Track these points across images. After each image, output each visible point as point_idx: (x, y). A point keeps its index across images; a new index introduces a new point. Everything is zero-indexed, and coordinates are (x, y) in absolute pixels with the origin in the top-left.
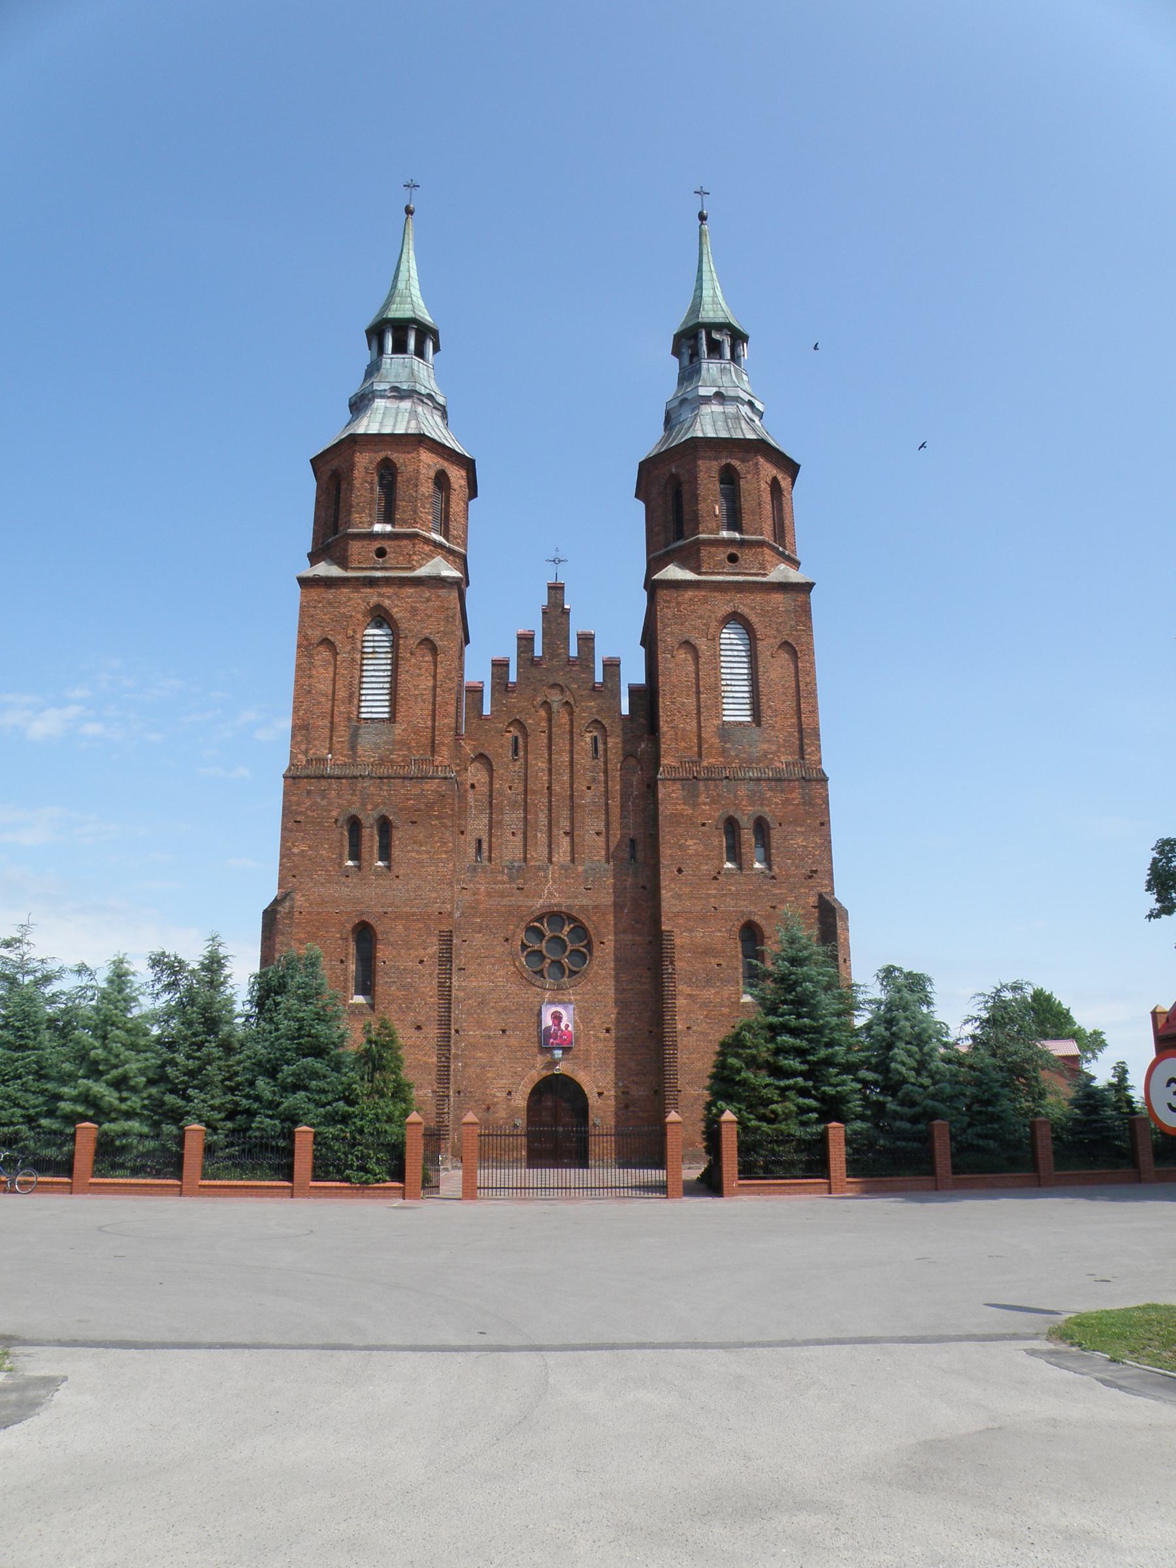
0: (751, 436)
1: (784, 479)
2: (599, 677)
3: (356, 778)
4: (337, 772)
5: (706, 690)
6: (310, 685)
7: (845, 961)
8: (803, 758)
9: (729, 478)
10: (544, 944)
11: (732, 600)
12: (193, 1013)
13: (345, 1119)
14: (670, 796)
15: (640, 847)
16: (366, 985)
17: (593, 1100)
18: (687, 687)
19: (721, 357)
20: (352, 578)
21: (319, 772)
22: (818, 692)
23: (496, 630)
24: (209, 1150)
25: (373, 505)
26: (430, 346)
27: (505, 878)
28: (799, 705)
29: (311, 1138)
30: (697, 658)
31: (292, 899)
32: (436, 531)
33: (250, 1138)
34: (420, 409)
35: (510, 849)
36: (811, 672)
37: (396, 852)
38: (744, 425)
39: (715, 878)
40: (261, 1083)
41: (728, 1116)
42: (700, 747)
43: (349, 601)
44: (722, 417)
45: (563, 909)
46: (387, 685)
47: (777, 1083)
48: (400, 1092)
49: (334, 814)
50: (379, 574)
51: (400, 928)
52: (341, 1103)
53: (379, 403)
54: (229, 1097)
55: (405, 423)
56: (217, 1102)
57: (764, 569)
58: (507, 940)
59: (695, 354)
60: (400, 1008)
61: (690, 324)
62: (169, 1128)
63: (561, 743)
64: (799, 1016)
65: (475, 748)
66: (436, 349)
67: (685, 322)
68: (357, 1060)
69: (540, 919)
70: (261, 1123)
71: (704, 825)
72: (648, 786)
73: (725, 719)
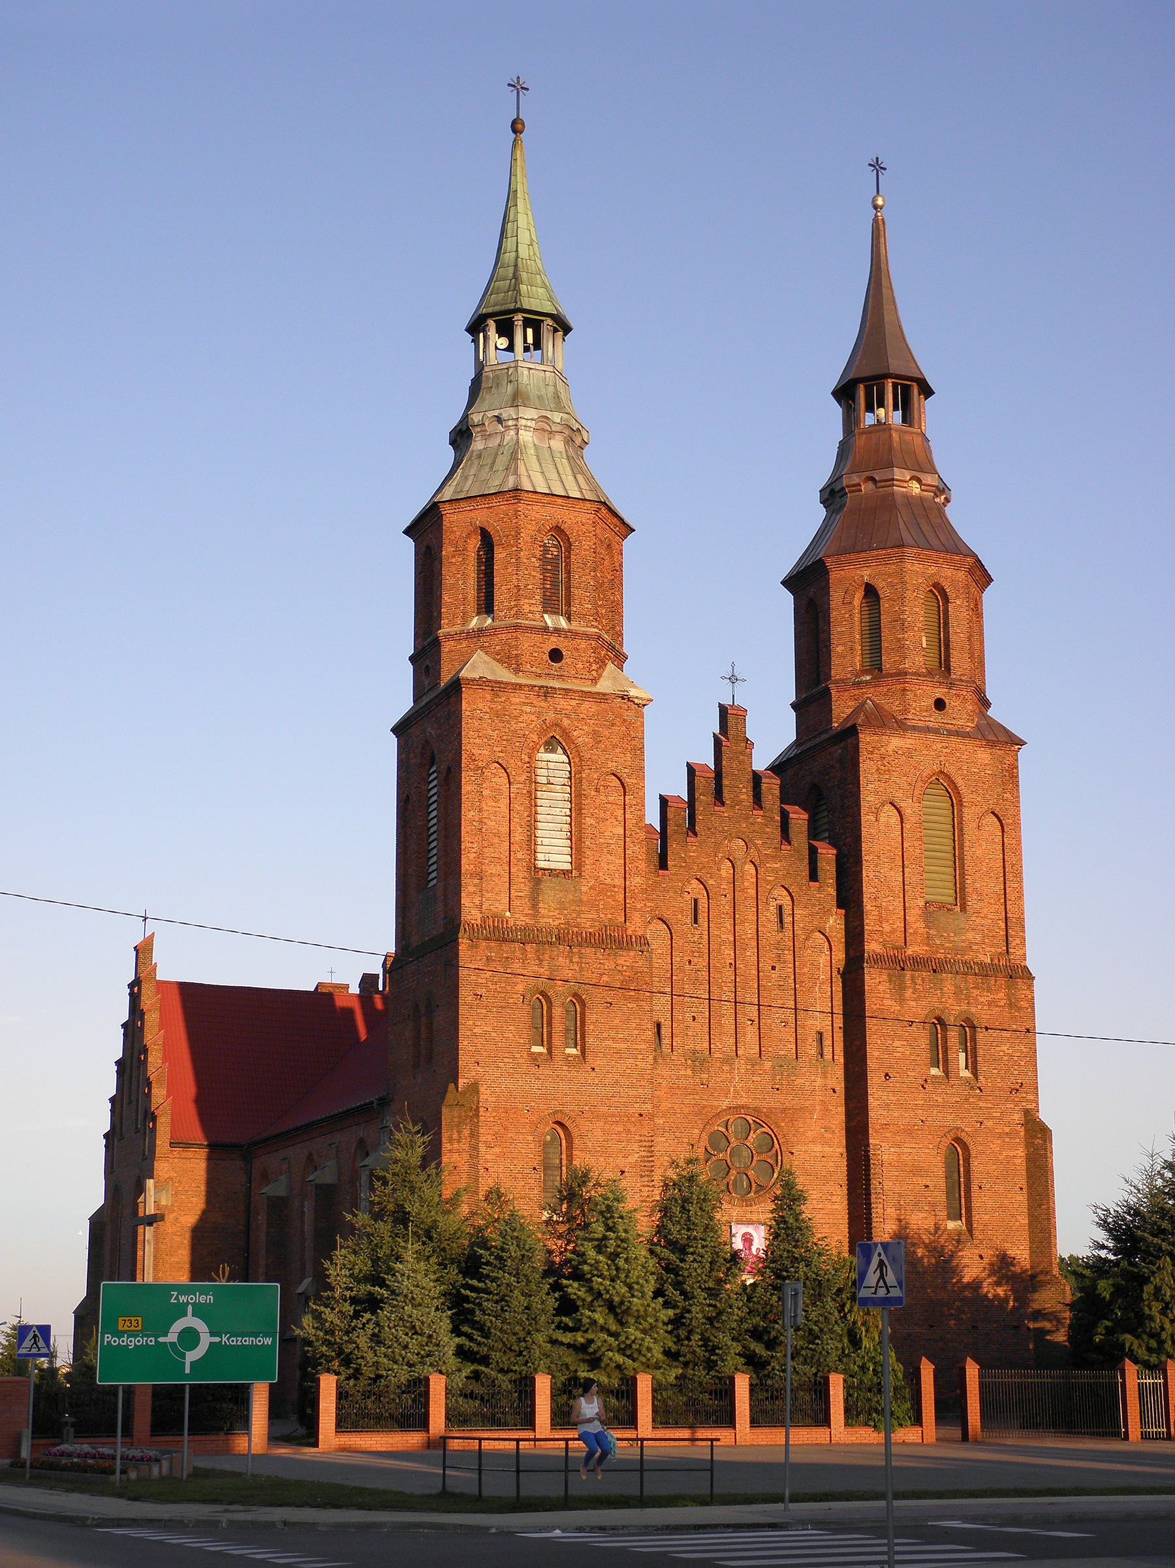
15: (827, 1042)
27: (689, 1072)
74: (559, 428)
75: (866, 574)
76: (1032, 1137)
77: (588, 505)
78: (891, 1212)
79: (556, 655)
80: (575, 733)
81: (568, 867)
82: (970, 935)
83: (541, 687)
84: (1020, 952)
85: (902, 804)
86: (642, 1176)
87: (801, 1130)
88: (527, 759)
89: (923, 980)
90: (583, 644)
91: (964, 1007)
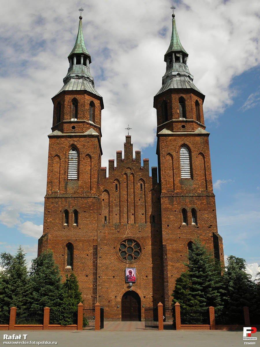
0: (188, 87)
1: (200, 100)
2: (142, 165)
3: (67, 198)
4: (61, 196)
5: (176, 168)
6: (52, 169)
7: (222, 254)
8: (207, 189)
9: (182, 101)
10: (126, 249)
11: (183, 140)
12: (14, 272)
13: (60, 305)
14: (165, 202)
16: (71, 262)
17: (142, 299)
18: (170, 168)
19: (180, 62)
20: (65, 136)
21: (55, 196)
22: (211, 168)
24: (18, 315)
25: (74, 113)
26: (88, 61)
27: (114, 228)
28: (205, 173)
29: (49, 311)
30: (172, 158)
31: (47, 236)
32: (91, 120)
33: (30, 311)
34: (85, 82)
35: (115, 219)
36: (209, 162)
37: (79, 221)
38: (187, 84)
39: (179, 228)
40: (34, 293)
41: (177, 304)
42: (174, 186)
43: (64, 143)
44: (180, 81)
45: (132, 238)
46: (76, 169)
47: (192, 293)
48: (77, 296)
49: (60, 209)
50: (73, 134)
51: (81, 245)
52: (58, 299)
53: (72, 80)
54: (24, 298)
55: (80, 87)
56: (21, 299)
57: (193, 130)
58: (114, 248)
60: (81, 270)
61: (170, 51)
62: (5, 308)
63: (131, 186)
64: (199, 272)
65: (104, 188)
66: (90, 62)
68: (64, 286)
69: (125, 241)
70: (34, 306)
71: (175, 211)
72: (158, 199)
73: (182, 177)
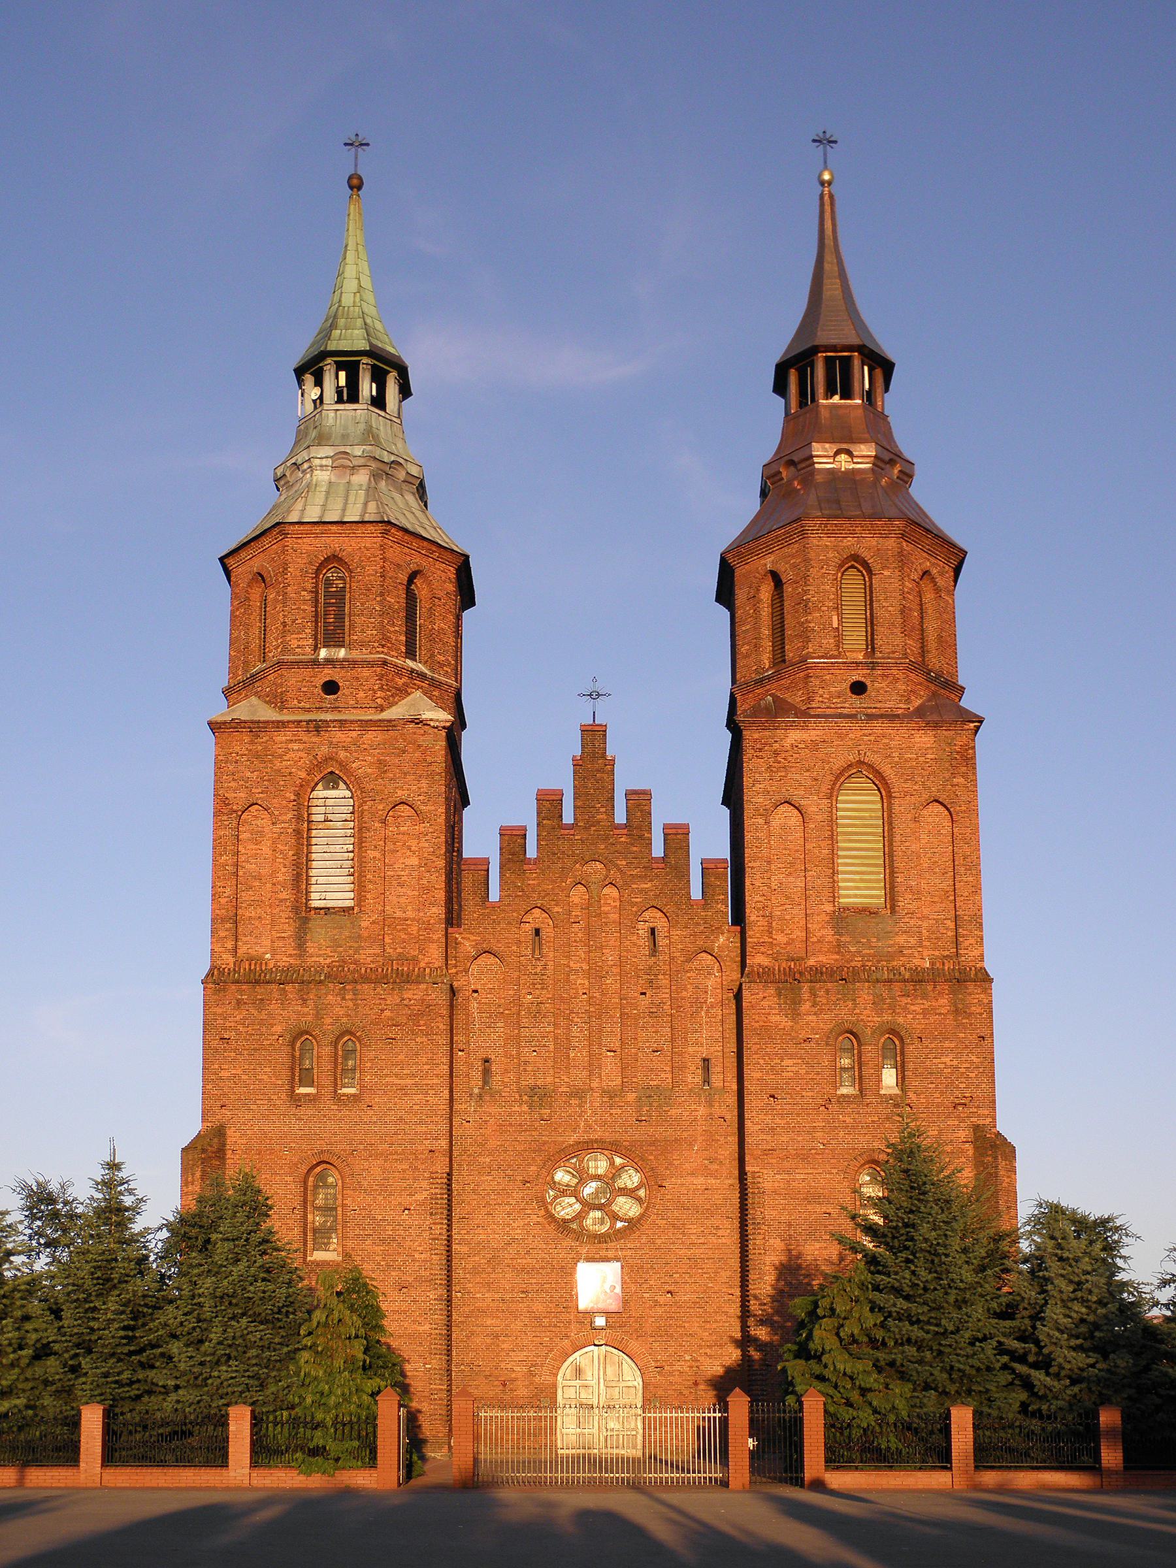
15: (716, 1069)
23: (511, 781)
27: (525, 1108)
55: (359, 506)
59: (806, 397)
66: (405, 391)
67: (785, 353)
74: (361, 461)
75: (769, 562)
76: (982, 1155)
77: (371, 528)
78: (777, 1243)
79: (331, 687)
80: (354, 765)
81: (350, 903)
82: (901, 940)
83: (308, 722)
84: (976, 953)
85: (803, 802)
86: (431, 1214)
87: (676, 1162)
88: (293, 797)
89: (827, 991)
90: (366, 673)
91: (887, 1017)
